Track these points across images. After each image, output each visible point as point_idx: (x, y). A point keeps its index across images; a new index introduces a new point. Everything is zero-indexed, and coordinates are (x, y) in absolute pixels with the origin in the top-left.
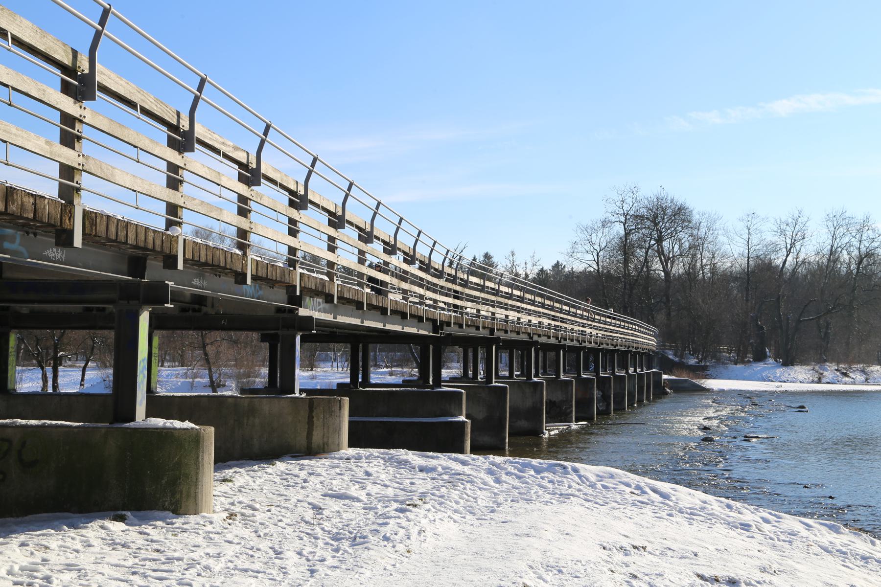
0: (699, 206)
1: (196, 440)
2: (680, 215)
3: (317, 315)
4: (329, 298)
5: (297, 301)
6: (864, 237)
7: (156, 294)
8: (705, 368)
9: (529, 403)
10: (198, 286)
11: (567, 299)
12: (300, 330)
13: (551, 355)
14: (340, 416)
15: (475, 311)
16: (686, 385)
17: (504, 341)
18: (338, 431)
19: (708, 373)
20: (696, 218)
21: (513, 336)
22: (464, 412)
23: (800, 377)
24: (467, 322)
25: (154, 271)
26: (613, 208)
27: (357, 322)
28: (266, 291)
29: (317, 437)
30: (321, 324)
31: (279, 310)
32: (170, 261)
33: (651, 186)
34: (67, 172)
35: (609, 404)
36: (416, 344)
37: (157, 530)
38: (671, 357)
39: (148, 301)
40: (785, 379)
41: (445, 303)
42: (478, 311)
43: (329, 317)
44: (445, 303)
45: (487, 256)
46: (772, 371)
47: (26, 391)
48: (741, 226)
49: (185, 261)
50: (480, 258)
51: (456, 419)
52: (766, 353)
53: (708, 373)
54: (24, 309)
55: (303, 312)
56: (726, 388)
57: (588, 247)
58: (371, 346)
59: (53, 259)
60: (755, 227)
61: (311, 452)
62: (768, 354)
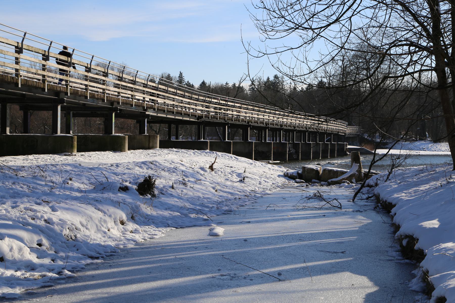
1: (124, 138)
3: (151, 114)
4: (154, 109)
5: (146, 110)
7: (115, 110)
10: (123, 108)
12: (72, 111)
13: (219, 130)
14: (157, 140)
15: (142, 98)
17: (298, 130)
18: (156, 143)
21: (275, 126)
22: (209, 148)
24: (211, 116)
25: (115, 105)
27: (173, 117)
28: (137, 108)
29: (151, 145)
30: (152, 116)
31: (141, 112)
32: (118, 103)
34: (17, 70)
36: (256, 130)
37: (118, 154)
39: (114, 111)
41: (37, 79)
42: (144, 98)
43: (155, 114)
44: (37, 79)
49: (70, 93)
50: (272, 79)
52: (426, 136)
54: (99, 112)
55: (147, 113)
59: (100, 104)
61: (149, 148)
62: (428, 136)
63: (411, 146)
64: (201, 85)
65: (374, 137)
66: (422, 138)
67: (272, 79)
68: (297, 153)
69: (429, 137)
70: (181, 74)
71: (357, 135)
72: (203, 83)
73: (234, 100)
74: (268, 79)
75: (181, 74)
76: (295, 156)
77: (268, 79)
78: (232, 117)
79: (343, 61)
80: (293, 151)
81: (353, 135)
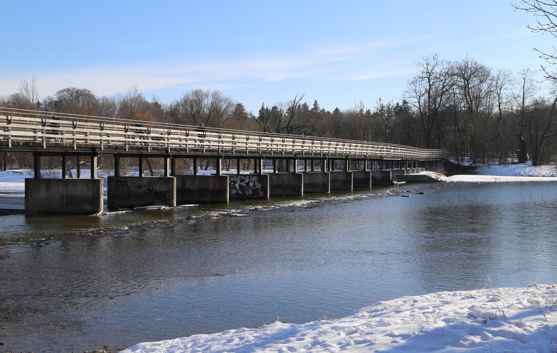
0: (493, 64)
2: (480, 73)
6: (455, 77)
8: (475, 168)
9: (90, 194)
11: (131, 122)
16: (425, 179)
19: (477, 170)
20: (494, 73)
23: (544, 173)
26: (422, 69)
33: (452, 54)
35: (266, 192)
38: (452, 161)
40: (532, 174)
45: (405, 102)
46: (523, 169)
47: (426, 184)
48: (520, 78)
50: (401, 104)
51: (309, 201)
52: (526, 158)
53: (477, 170)
56: (534, 180)
57: (414, 94)
58: (143, 158)
60: (529, 77)
62: (528, 158)
63: (505, 169)
64: (334, 112)
65: (462, 160)
66: (522, 160)
67: (401, 104)
68: (264, 189)
69: (530, 160)
70: (316, 102)
71: (440, 158)
72: (337, 110)
73: (88, 118)
74: (398, 104)
75: (316, 102)
76: (261, 194)
77: (398, 104)
78: (101, 143)
79: (429, 78)
80: (259, 186)
81: (433, 158)
